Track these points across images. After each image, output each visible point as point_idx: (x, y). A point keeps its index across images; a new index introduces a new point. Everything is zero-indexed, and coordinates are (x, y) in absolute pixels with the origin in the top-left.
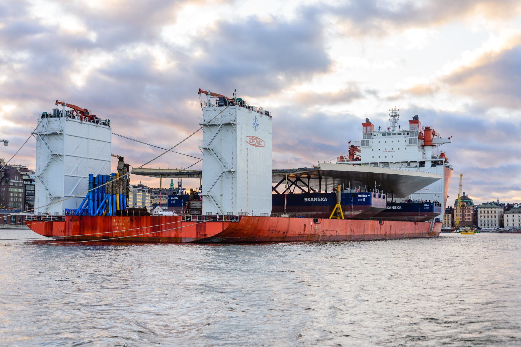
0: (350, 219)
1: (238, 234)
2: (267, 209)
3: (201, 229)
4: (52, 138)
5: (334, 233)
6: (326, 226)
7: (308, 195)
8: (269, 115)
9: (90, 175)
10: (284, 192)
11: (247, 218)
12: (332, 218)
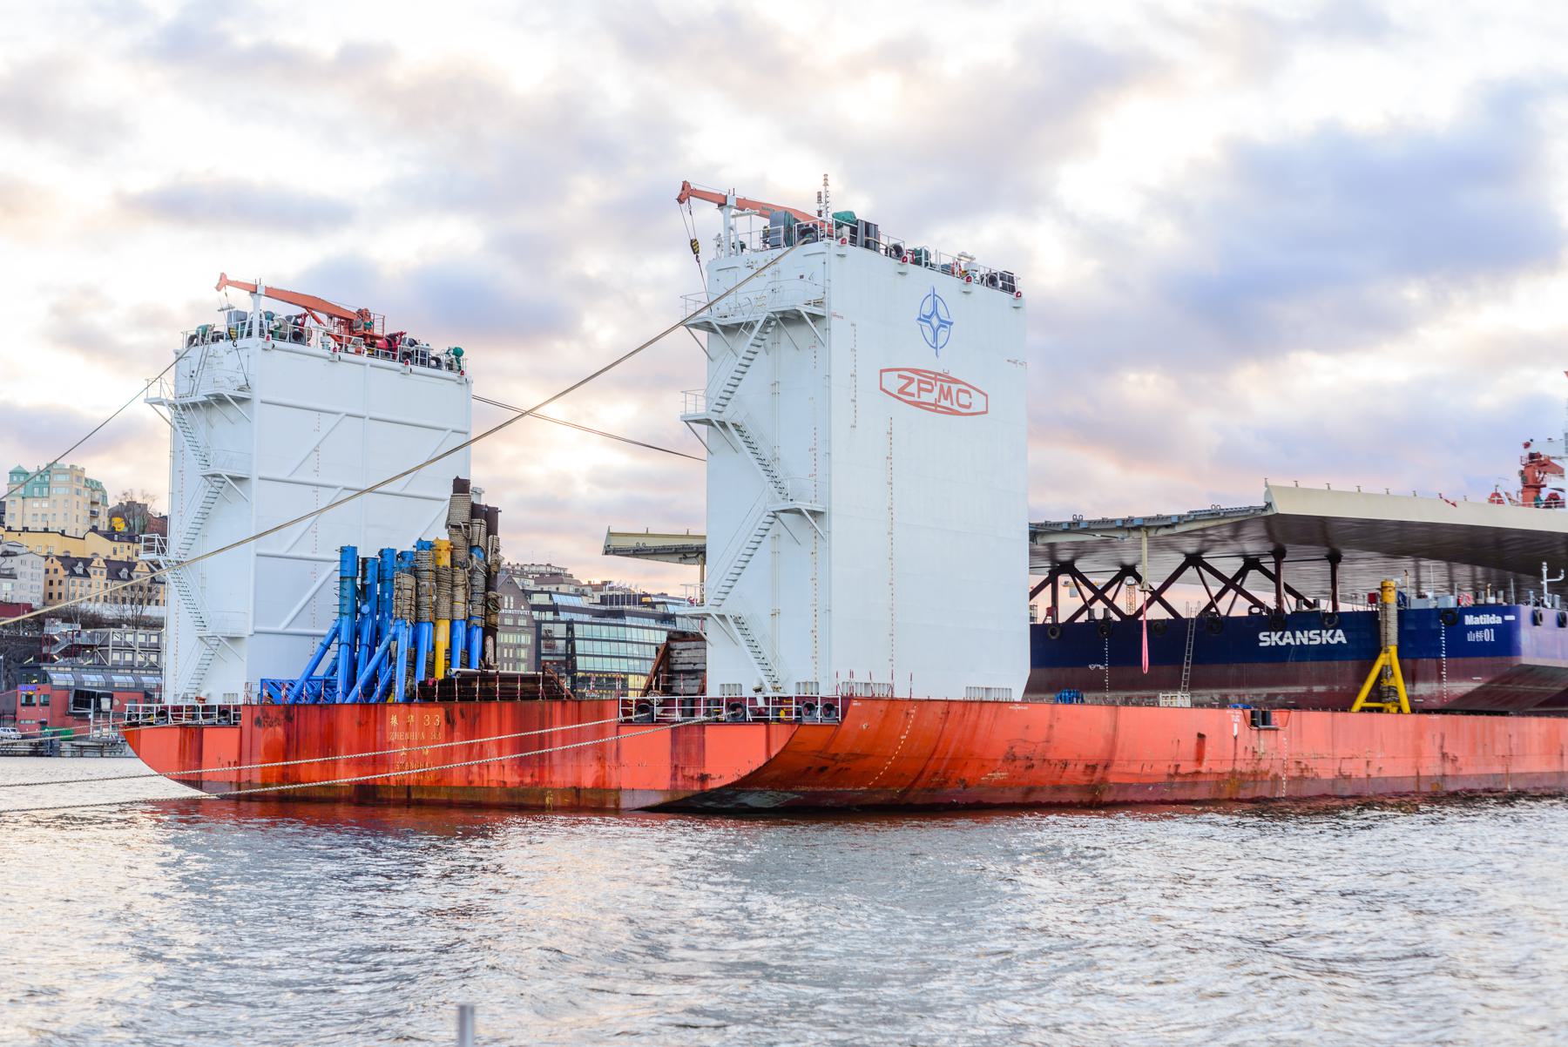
0: (1437, 711)
1: (844, 778)
2: (1009, 671)
3: (687, 754)
4: (217, 415)
5: (1357, 769)
6: (1309, 741)
7: (1277, 620)
8: (1012, 290)
9: (343, 550)
10: (1140, 612)
11: (882, 706)
12: (1363, 710)
